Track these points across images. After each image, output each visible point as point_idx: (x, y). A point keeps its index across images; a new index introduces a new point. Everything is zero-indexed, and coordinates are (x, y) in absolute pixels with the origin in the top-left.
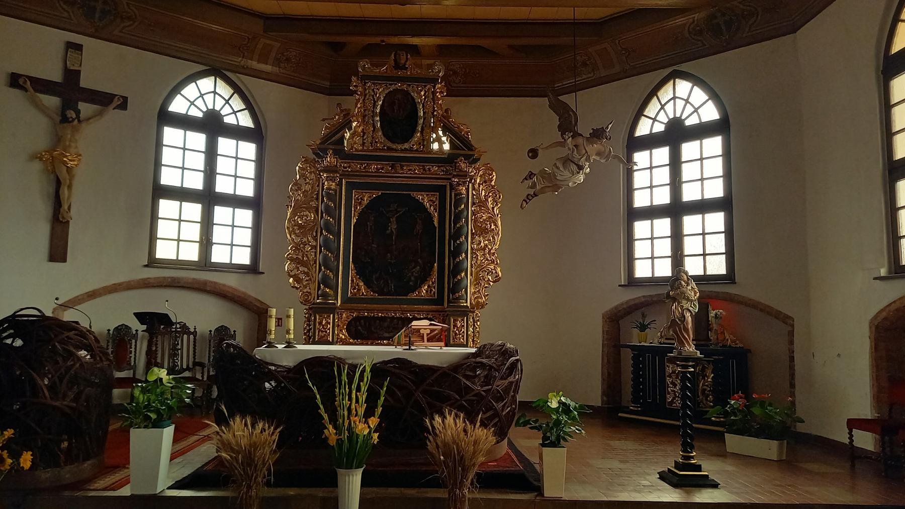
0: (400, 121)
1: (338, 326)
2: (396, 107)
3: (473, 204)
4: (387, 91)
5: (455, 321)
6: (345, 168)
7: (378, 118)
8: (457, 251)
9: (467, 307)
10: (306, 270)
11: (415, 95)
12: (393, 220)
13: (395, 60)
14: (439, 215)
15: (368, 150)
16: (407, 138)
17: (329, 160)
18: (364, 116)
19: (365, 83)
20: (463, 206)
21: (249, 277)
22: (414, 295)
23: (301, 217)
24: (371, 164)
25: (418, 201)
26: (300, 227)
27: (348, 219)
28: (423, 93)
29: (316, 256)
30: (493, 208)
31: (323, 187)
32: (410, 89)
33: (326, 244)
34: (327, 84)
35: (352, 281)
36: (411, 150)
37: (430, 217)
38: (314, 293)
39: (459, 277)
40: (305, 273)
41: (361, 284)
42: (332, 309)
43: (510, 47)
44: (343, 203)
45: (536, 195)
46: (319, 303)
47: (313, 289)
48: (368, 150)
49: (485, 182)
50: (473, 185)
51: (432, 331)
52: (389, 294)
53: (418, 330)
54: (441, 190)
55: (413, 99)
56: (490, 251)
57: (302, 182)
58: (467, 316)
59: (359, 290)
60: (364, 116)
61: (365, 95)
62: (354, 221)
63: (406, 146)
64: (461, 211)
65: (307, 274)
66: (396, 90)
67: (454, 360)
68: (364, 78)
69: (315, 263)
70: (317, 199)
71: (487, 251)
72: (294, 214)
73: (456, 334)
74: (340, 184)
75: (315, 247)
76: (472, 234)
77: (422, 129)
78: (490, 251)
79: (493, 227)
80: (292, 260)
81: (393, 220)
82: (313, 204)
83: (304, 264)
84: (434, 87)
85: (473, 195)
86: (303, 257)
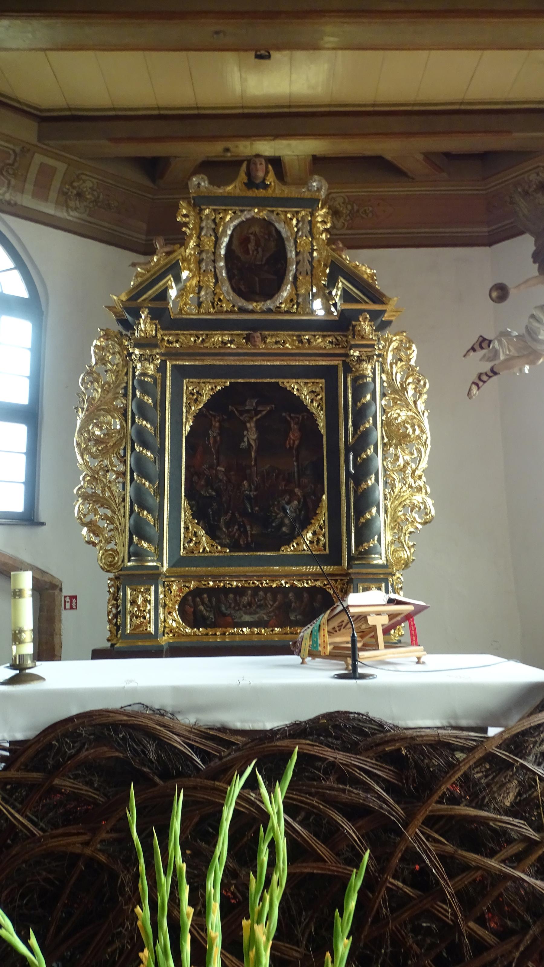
0: (257, 266)
1: (165, 605)
2: (251, 246)
3: (384, 395)
4: (236, 222)
6: (169, 342)
7: (222, 264)
8: (363, 469)
10: (109, 513)
11: (281, 227)
12: (251, 425)
13: (248, 173)
14: (327, 416)
16: (271, 290)
17: (145, 326)
18: (200, 262)
19: (201, 210)
20: (368, 397)
21: (21, 532)
22: (290, 550)
24: (213, 336)
25: (291, 393)
26: (98, 441)
28: (294, 222)
29: (124, 488)
30: (415, 402)
31: (134, 372)
32: (273, 217)
33: (140, 466)
35: (187, 528)
37: (311, 418)
38: (124, 551)
39: (368, 516)
40: (107, 518)
41: (202, 533)
42: (152, 577)
44: (168, 390)
45: (494, 372)
46: (131, 568)
48: (209, 313)
49: (401, 360)
50: (382, 365)
51: (392, 616)
52: (248, 548)
53: (363, 618)
54: (329, 374)
55: (278, 232)
56: (413, 472)
57: (100, 368)
58: (386, 581)
59: (197, 543)
60: (200, 262)
63: (269, 304)
64: (366, 406)
65: (111, 521)
66: (252, 221)
68: (198, 203)
69: (124, 500)
70: (125, 395)
71: (409, 471)
75: (124, 474)
76: (384, 445)
77: (295, 278)
78: (413, 472)
79: (418, 432)
80: (86, 497)
82: (119, 403)
83: (103, 502)
84: (312, 214)
85: (382, 381)
86: (103, 491)
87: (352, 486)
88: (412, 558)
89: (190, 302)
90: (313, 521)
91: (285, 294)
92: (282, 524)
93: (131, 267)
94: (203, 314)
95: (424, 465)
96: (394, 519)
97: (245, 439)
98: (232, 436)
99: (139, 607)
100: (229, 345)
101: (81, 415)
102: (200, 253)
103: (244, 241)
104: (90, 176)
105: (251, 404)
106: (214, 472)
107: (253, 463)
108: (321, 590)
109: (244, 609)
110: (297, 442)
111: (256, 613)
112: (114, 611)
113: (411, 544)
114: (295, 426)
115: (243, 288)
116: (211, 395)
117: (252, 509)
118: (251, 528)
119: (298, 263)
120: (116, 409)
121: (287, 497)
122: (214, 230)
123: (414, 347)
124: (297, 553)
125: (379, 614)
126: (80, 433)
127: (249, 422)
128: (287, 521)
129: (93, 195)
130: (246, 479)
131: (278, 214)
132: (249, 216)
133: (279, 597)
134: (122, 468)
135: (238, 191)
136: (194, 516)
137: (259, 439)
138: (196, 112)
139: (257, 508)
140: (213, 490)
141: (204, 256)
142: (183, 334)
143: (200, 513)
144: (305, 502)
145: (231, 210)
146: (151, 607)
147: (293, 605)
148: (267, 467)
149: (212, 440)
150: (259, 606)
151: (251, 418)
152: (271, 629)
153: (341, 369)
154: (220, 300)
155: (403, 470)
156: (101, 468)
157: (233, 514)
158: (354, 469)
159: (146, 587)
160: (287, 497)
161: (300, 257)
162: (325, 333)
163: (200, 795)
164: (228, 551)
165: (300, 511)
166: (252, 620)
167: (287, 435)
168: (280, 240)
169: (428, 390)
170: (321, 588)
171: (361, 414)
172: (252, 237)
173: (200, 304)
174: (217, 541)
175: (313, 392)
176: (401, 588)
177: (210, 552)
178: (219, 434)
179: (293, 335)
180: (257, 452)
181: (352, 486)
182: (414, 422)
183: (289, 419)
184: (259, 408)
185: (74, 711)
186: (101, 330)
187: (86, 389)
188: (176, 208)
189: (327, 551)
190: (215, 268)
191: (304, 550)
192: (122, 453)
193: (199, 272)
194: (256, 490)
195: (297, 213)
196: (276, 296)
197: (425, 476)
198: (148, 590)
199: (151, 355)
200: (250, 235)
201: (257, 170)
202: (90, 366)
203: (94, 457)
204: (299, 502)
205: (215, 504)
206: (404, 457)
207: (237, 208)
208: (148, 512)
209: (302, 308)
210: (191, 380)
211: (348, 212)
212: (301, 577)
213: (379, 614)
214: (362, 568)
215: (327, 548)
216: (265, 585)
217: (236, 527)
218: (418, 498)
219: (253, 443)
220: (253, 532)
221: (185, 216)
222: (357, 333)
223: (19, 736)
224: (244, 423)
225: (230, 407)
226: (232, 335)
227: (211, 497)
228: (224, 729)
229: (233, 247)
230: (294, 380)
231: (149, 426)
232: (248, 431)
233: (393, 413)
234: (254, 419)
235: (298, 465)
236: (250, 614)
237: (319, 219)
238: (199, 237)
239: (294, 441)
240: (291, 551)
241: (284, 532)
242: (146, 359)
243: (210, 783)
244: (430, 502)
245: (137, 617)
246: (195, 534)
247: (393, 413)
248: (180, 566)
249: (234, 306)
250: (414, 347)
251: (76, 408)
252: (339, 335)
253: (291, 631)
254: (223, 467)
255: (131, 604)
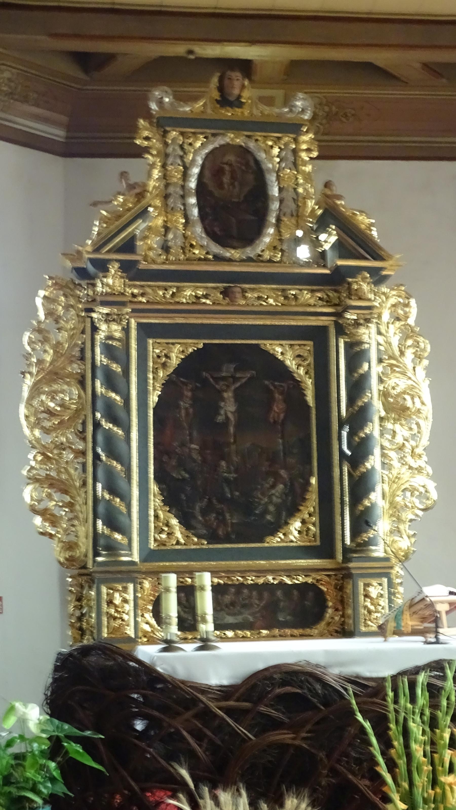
0: (235, 204)
2: (226, 179)
3: (380, 361)
5: (367, 585)
8: (361, 450)
9: (133, 563)
11: (262, 156)
12: (228, 395)
13: (221, 89)
15: (178, 262)
18: (166, 197)
19: (165, 133)
22: (275, 541)
23: (52, 395)
26: (51, 413)
27: (144, 393)
28: (276, 151)
32: (252, 145)
34: (57, 133)
35: (156, 517)
36: (258, 260)
37: (297, 386)
41: (174, 522)
43: (426, 66)
47: (83, 532)
48: (178, 262)
49: (398, 319)
59: (170, 534)
61: (167, 156)
62: (153, 399)
63: (250, 252)
65: (71, 505)
67: (78, 735)
68: (163, 124)
71: (408, 449)
72: (36, 390)
73: (370, 612)
74: (126, 330)
75: (83, 453)
77: (279, 220)
80: (35, 480)
81: (228, 395)
82: (75, 368)
84: (296, 140)
87: (346, 469)
88: (413, 549)
89: (156, 246)
90: (301, 508)
91: (267, 240)
92: (266, 512)
93: (92, 208)
94: (172, 263)
95: (425, 441)
96: (393, 505)
97: (222, 412)
98: (207, 409)
99: (116, 606)
100: (204, 301)
101: (29, 381)
102: (167, 185)
103: (218, 173)
104: (9, 66)
105: (228, 369)
106: (187, 450)
107: (232, 440)
108: (313, 587)
109: (227, 609)
110: (282, 416)
111: (240, 613)
112: (78, 613)
113: (412, 533)
114: (280, 397)
115: (216, 229)
116: (182, 359)
117: (232, 494)
118: (231, 516)
119: (281, 201)
120: (70, 375)
121: (271, 480)
122: (182, 157)
123: (413, 302)
124: (285, 544)
125: (442, 602)
126: (29, 403)
127: (226, 391)
128: (271, 508)
129: (10, 87)
130: (223, 459)
131: (257, 140)
132: (222, 142)
133: (266, 595)
134: (80, 446)
135: (209, 111)
136: (165, 502)
137: (238, 412)
138: (158, 9)
139: (237, 493)
140: (185, 470)
141: (171, 190)
142: (149, 286)
143: (171, 500)
144: (292, 485)
145: (202, 133)
146: (129, 607)
147: (282, 604)
148: (248, 445)
149: (183, 413)
150: (244, 606)
151: (228, 386)
152: (258, 632)
153: (332, 332)
154: (192, 246)
155: (401, 448)
156: (56, 447)
157: (209, 499)
158: (349, 448)
159: (125, 585)
160: (271, 480)
161: (284, 194)
162: (315, 288)
163: (366, 707)
164: (206, 543)
165: (286, 495)
166: (236, 621)
167: (269, 408)
168: (259, 173)
169: (430, 353)
170: (313, 585)
171: (357, 386)
172: (227, 168)
173: (166, 249)
174: (193, 531)
175: (299, 356)
176: (401, 584)
177: (185, 544)
178: (192, 406)
179: (277, 289)
180: (236, 427)
181: (346, 469)
182: (412, 391)
183: (272, 388)
184: (238, 375)
185: (261, 666)
186: (51, 278)
187: (33, 349)
188: (134, 130)
189: (318, 543)
190: (184, 205)
191: (292, 541)
192: (80, 428)
193: (167, 209)
194: (236, 471)
195: (279, 138)
196: (257, 242)
197: (426, 455)
198: (125, 589)
199: (118, 315)
200: (225, 166)
201: (233, 87)
202: (39, 322)
203: (46, 431)
204: (285, 485)
205: (188, 489)
206: (402, 432)
207: (208, 131)
208: (122, 500)
209: (288, 256)
210: (158, 341)
211: (325, 114)
212: (290, 572)
213: (442, 602)
214: (363, 561)
215: (318, 539)
216: (250, 582)
217: (214, 515)
218: (419, 481)
219: (230, 415)
220: (234, 521)
221: (147, 138)
222: (353, 292)
223: (225, 682)
224: (220, 392)
225: (204, 373)
226: (207, 288)
227: (184, 479)
228: (358, 677)
229: (205, 180)
230: (278, 342)
231: (118, 398)
232: (226, 403)
233: (391, 382)
234: (233, 388)
235: (283, 444)
236: (234, 615)
237: (304, 147)
238: (164, 166)
239: (279, 414)
240: (278, 542)
241: (270, 521)
242: (114, 320)
243: (370, 700)
244: (431, 485)
245: (115, 618)
246: (167, 525)
247: (391, 382)
248: (151, 561)
249: (208, 253)
250: (413, 302)
251: (23, 373)
252: (329, 290)
253: (280, 633)
254: (197, 445)
255: (108, 605)
